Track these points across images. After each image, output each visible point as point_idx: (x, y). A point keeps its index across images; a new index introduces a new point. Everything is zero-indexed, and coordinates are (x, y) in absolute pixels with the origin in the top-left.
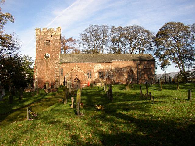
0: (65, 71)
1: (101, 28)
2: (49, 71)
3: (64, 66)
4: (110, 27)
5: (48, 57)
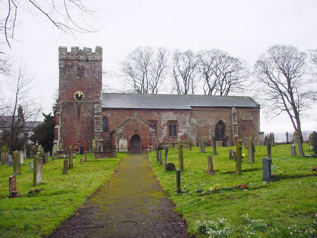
2: (83, 123)
3: (109, 115)
4: (173, 52)
5: (80, 98)
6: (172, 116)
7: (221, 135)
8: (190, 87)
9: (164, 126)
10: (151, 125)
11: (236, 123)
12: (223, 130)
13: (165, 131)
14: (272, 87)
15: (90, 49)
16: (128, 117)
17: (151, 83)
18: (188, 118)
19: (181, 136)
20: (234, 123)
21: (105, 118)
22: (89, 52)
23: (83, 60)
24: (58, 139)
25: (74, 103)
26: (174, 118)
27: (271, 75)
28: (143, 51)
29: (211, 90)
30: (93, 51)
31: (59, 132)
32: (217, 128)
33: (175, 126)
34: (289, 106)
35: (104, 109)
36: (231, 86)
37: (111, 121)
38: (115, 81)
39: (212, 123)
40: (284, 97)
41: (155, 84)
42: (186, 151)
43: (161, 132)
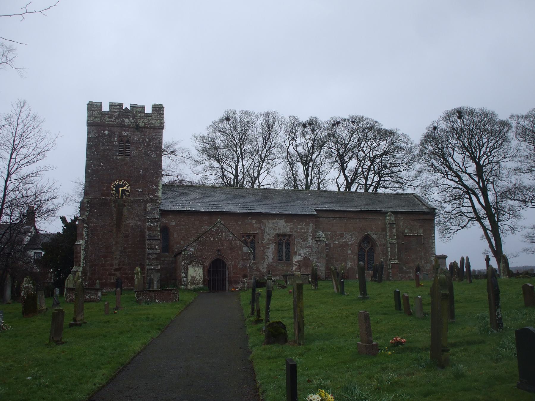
0: (175, 237)
1: (260, 121)
6: (283, 226)
7: (370, 265)
8: (315, 180)
9: (268, 244)
10: (245, 242)
11: (394, 240)
12: (372, 250)
13: (270, 253)
14: (452, 180)
15: (143, 108)
16: (205, 227)
17: (251, 172)
18: (310, 231)
19: (298, 262)
20: (390, 240)
21: (165, 230)
22: (141, 112)
23: (129, 127)
24: (79, 265)
25: (111, 200)
26: (288, 230)
27: (450, 160)
28: (239, 120)
29: (349, 185)
30: (148, 110)
31: (82, 252)
32: (361, 248)
33: (288, 245)
34: (482, 212)
35: (165, 213)
36: (382, 179)
37: (175, 233)
38: (184, 161)
39: (352, 239)
40: (474, 198)
41: (256, 175)
42: (308, 290)
43: (264, 253)
